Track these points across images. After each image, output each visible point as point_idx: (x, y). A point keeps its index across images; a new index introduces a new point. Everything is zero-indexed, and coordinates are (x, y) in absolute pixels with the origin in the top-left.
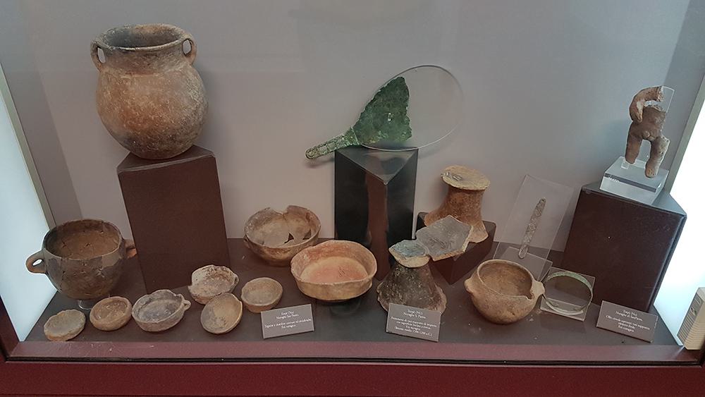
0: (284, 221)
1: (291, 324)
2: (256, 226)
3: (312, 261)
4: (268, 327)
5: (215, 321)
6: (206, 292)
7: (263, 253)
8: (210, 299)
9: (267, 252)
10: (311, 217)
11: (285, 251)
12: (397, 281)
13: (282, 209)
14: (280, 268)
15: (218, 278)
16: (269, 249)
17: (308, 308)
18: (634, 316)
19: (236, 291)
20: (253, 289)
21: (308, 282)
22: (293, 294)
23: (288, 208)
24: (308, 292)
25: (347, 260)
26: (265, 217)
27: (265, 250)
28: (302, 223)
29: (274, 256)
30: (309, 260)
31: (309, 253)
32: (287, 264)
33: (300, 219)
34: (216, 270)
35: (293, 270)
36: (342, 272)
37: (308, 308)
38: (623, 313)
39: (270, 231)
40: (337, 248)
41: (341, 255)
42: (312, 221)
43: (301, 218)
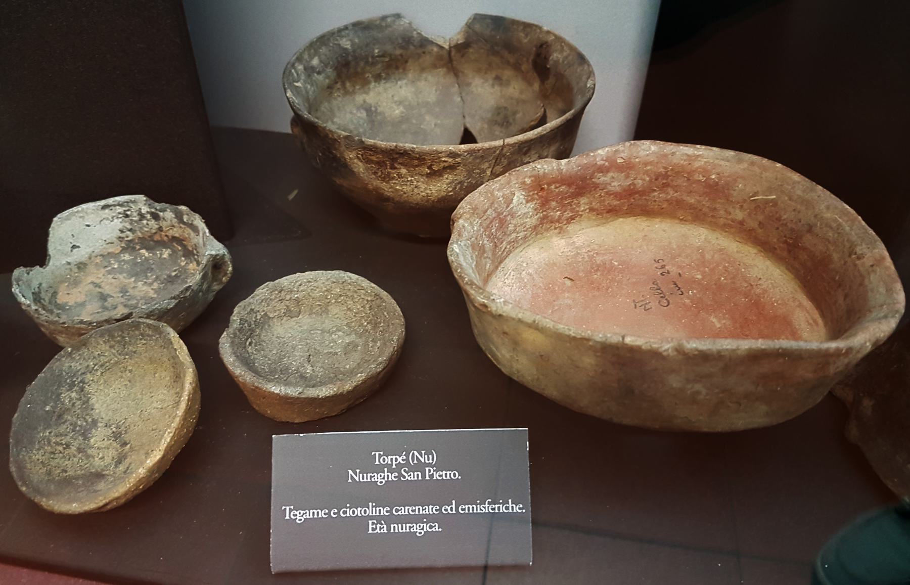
0: (450, 79)
1: (418, 519)
2: (339, 76)
3: (545, 224)
4: (300, 516)
5: (85, 435)
6: (103, 297)
7: (344, 168)
8: (81, 334)
9: (359, 167)
10: (555, 56)
11: (429, 164)
12: (496, 123)
13: (444, 25)
14: (403, 244)
15: (166, 253)
16: (368, 152)
17: (512, 442)
18: (420, 467)
19: (200, 321)
20: (289, 314)
21: (528, 317)
22: (444, 368)
23: (469, 26)
24: (515, 362)
25: (699, 236)
26: (374, 53)
27: (350, 156)
28: (518, 90)
29: (386, 188)
30: (534, 221)
31: (540, 189)
32: (436, 222)
33: (508, 73)
34: (155, 217)
35: (459, 252)
36: (667, 286)
37: (512, 442)
38: (379, 469)
39: (398, 111)
40: (664, 178)
41: (675, 210)
42: (560, 76)
43: (516, 67)
